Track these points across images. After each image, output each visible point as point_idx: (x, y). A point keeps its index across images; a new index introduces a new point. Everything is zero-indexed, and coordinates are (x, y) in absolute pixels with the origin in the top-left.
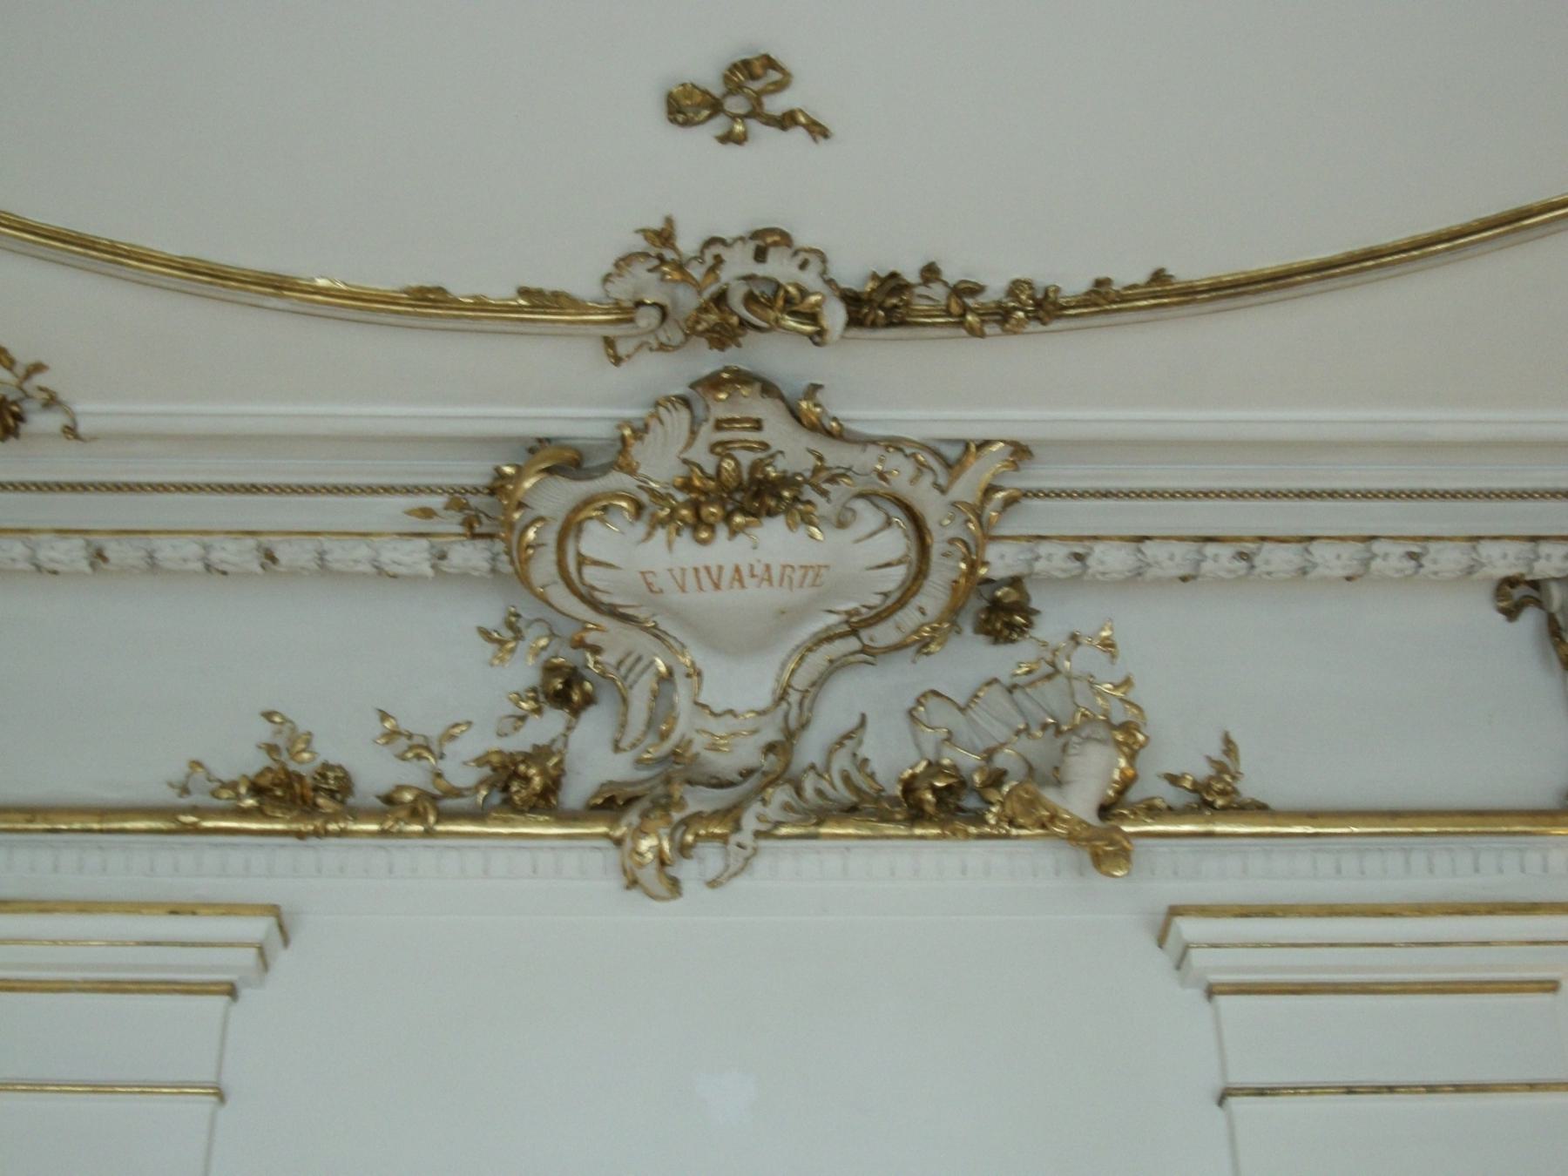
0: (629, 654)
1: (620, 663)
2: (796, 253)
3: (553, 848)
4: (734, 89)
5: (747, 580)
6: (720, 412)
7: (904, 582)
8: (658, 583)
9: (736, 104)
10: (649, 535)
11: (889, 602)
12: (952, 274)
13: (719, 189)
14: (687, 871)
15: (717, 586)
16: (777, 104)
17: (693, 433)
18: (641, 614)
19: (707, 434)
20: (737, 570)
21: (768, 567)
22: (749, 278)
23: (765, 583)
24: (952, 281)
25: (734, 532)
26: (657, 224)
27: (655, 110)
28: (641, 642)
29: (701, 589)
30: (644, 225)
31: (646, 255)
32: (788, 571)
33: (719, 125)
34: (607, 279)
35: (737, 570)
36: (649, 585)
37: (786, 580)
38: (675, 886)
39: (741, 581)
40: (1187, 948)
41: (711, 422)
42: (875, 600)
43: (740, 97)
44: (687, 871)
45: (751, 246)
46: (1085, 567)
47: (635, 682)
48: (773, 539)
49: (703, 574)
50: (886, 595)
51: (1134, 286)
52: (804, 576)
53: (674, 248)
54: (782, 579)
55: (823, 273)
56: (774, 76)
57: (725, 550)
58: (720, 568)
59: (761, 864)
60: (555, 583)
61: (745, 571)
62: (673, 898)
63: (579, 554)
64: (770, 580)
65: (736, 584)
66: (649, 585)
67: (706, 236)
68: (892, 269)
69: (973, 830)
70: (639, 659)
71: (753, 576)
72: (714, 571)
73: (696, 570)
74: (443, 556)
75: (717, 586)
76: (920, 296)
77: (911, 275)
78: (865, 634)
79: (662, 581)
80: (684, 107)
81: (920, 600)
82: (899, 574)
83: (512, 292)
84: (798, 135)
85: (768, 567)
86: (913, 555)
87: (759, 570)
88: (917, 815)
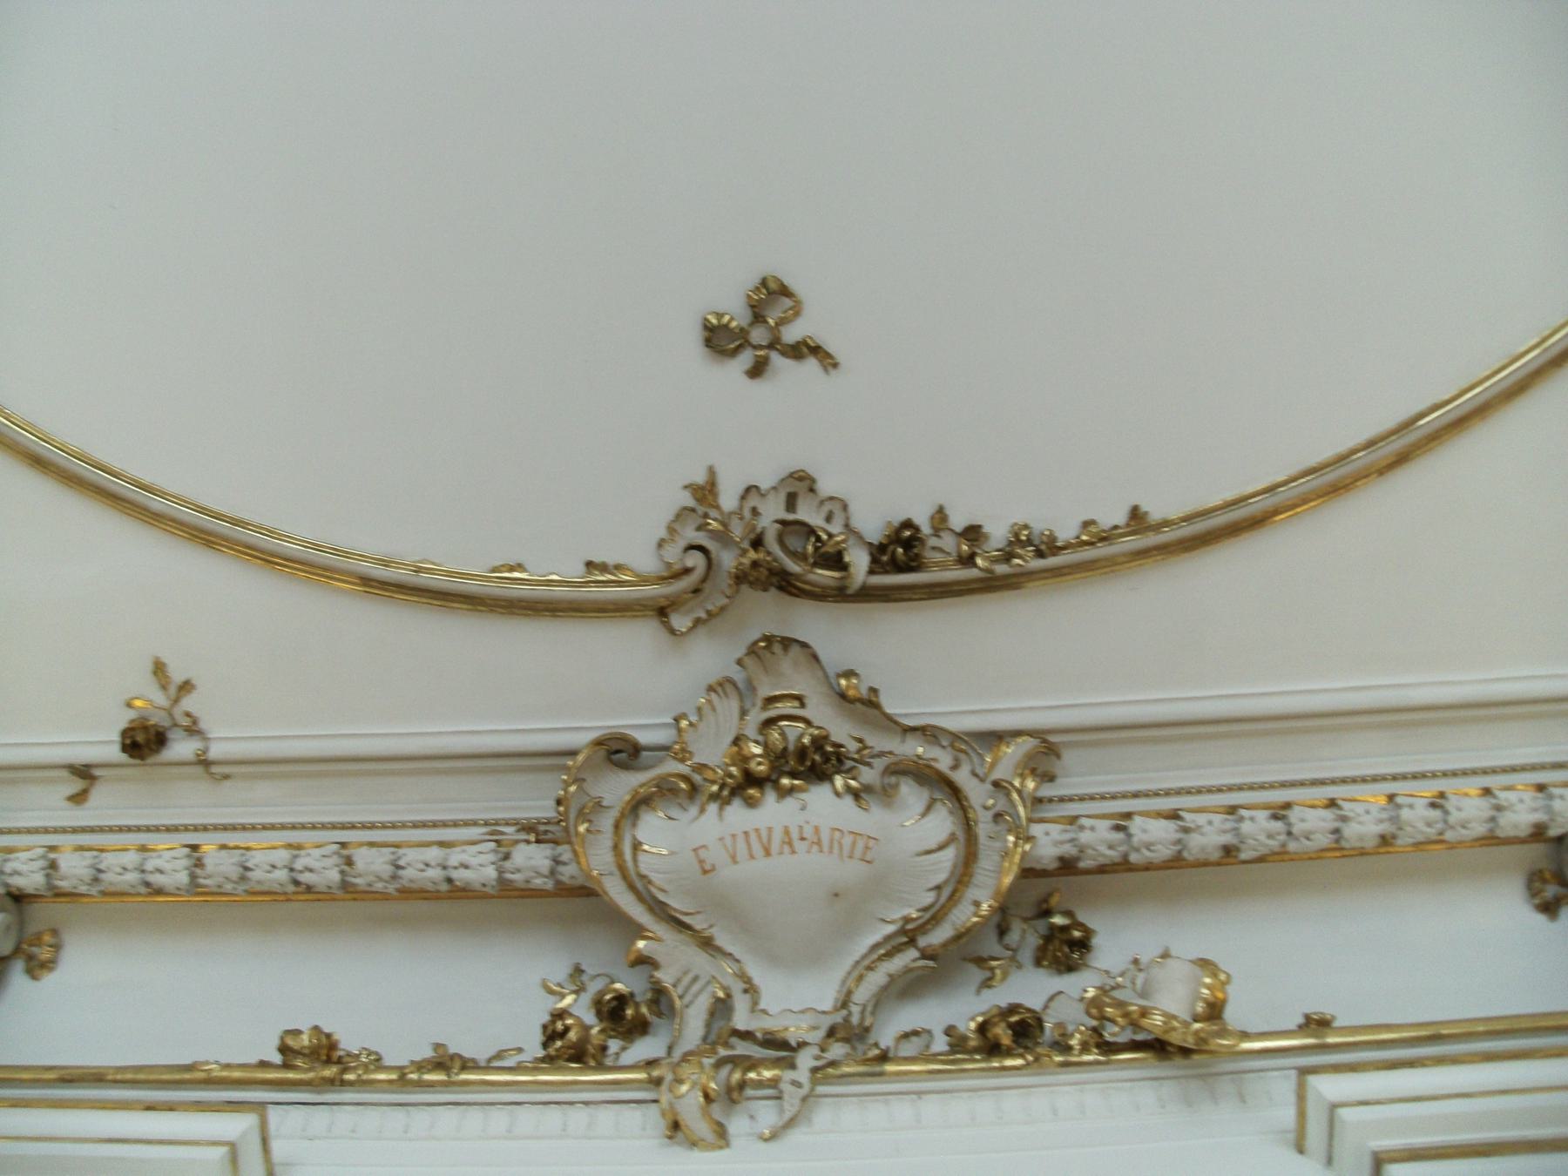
0: (686, 973)
1: (679, 980)
2: (822, 502)
3: (586, 1103)
4: (758, 317)
5: (797, 844)
6: (766, 691)
7: (955, 866)
8: (709, 857)
9: (758, 335)
10: (702, 811)
11: (946, 893)
12: (958, 521)
13: (755, 434)
14: (738, 1125)
15: (768, 853)
16: (791, 334)
17: (743, 713)
18: (697, 922)
19: (756, 716)
20: (787, 832)
21: (817, 829)
22: (783, 523)
23: (815, 848)
24: (959, 529)
25: (785, 793)
26: (700, 478)
27: (693, 338)
28: (700, 961)
29: (752, 857)
30: (687, 482)
31: (693, 510)
32: (837, 834)
33: (746, 359)
34: (661, 544)
35: (787, 832)
36: (701, 862)
37: (836, 845)
38: (722, 1133)
39: (790, 844)
40: (1334, 1107)
41: (759, 703)
42: (929, 898)
43: (758, 333)
44: (738, 1125)
45: (782, 497)
46: (1129, 836)
47: (691, 1002)
48: (823, 805)
49: (753, 836)
50: (938, 888)
51: (1116, 527)
52: (854, 844)
53: (718, 507)
54: (831, 847)
55: (847, 526)
56: (788, 303)
57: (773, 812)
58: (770, 829)
59: (823, 1115)
60: (611, 874)
61: (795, 835)
62: (721, 1148)
63: (634, 838)
64: (819, 843)
65: (786, 849)
66: (701, 862)
67: (744, 486)
68: (902, 517)
69: (1059, 1059)
70: (696, 979)
71: (803, 839)
72: (764, 834)
73: (746, 833)
74: (507, 857)
75: (768, 853)
76: (934, 548)
77: (923, 521)
78: (923, 942)
79: (715, 855)
80: (719, 339)
81: (972, 893)
82: (949, 854)
83: (576, 571)
84: (812, 364)
85: (817, 829)
86: (960, 835)
87: (808, 831)
88: (993, 1049)
